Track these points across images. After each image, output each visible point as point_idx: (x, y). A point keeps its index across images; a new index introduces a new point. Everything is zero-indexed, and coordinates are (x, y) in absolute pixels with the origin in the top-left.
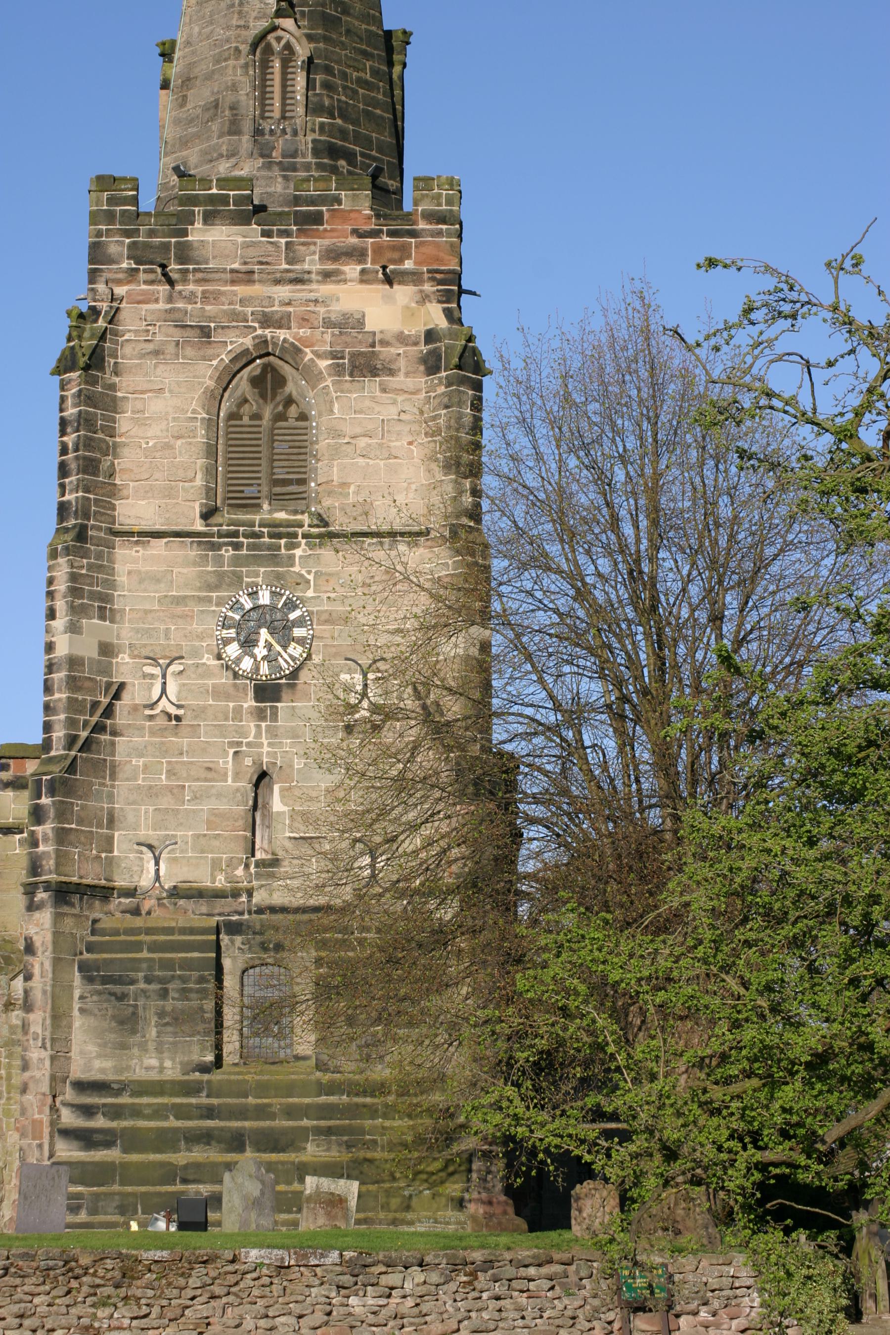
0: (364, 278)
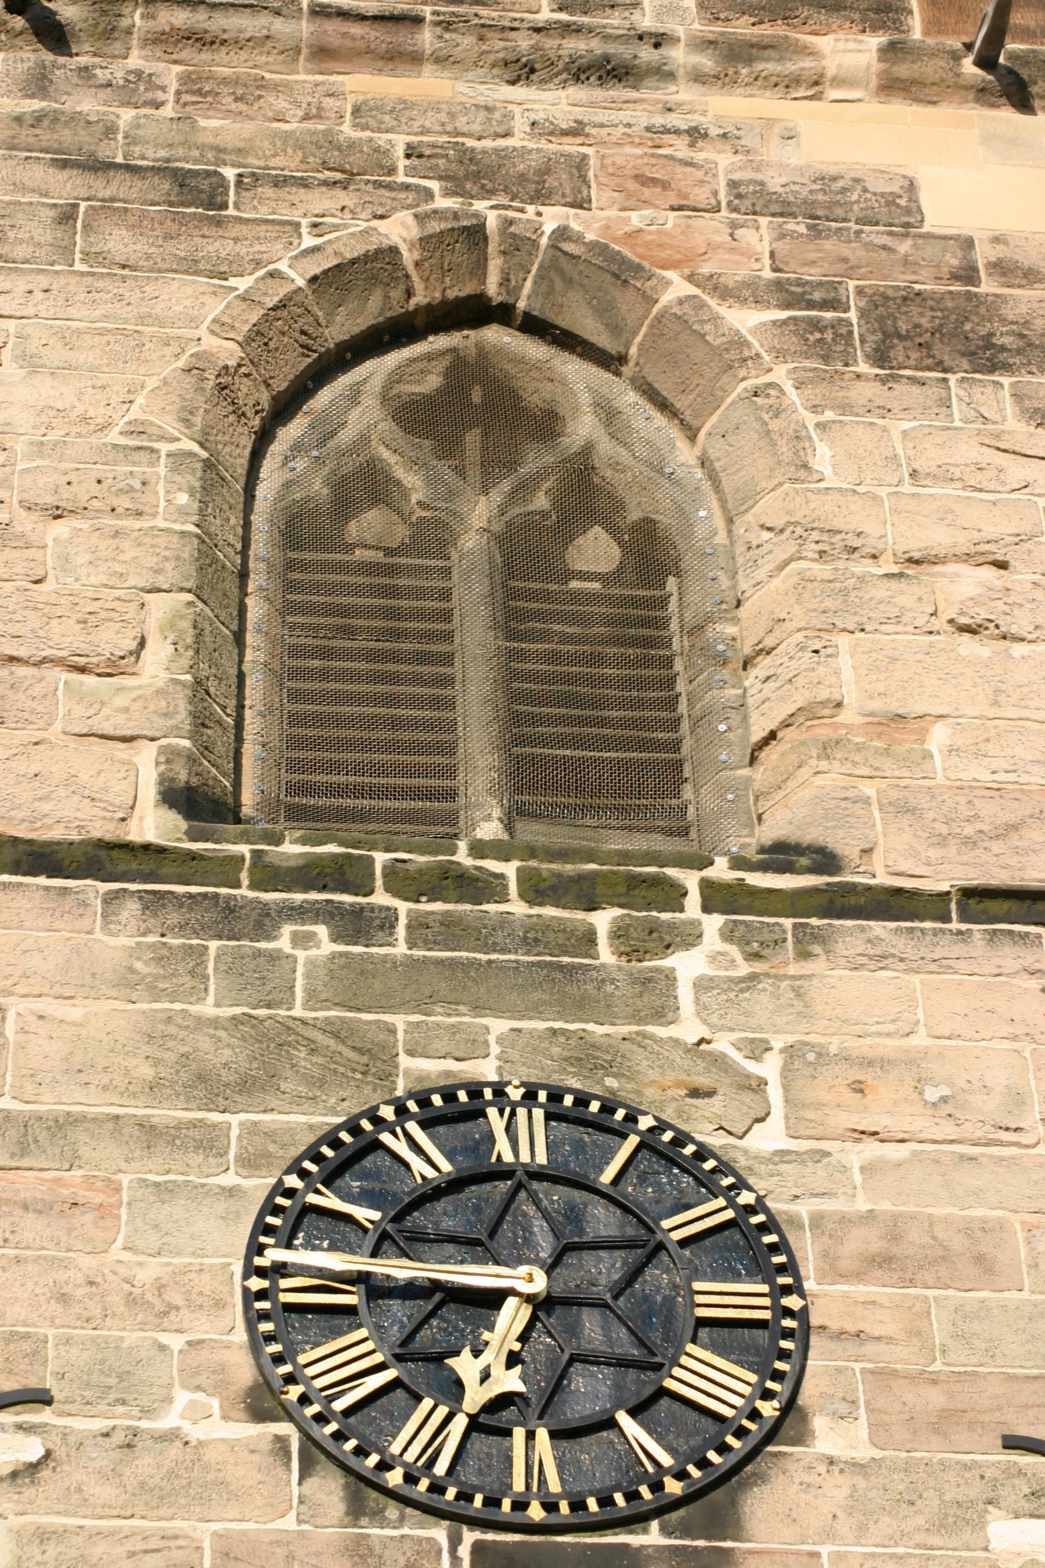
0: (903, 70)
